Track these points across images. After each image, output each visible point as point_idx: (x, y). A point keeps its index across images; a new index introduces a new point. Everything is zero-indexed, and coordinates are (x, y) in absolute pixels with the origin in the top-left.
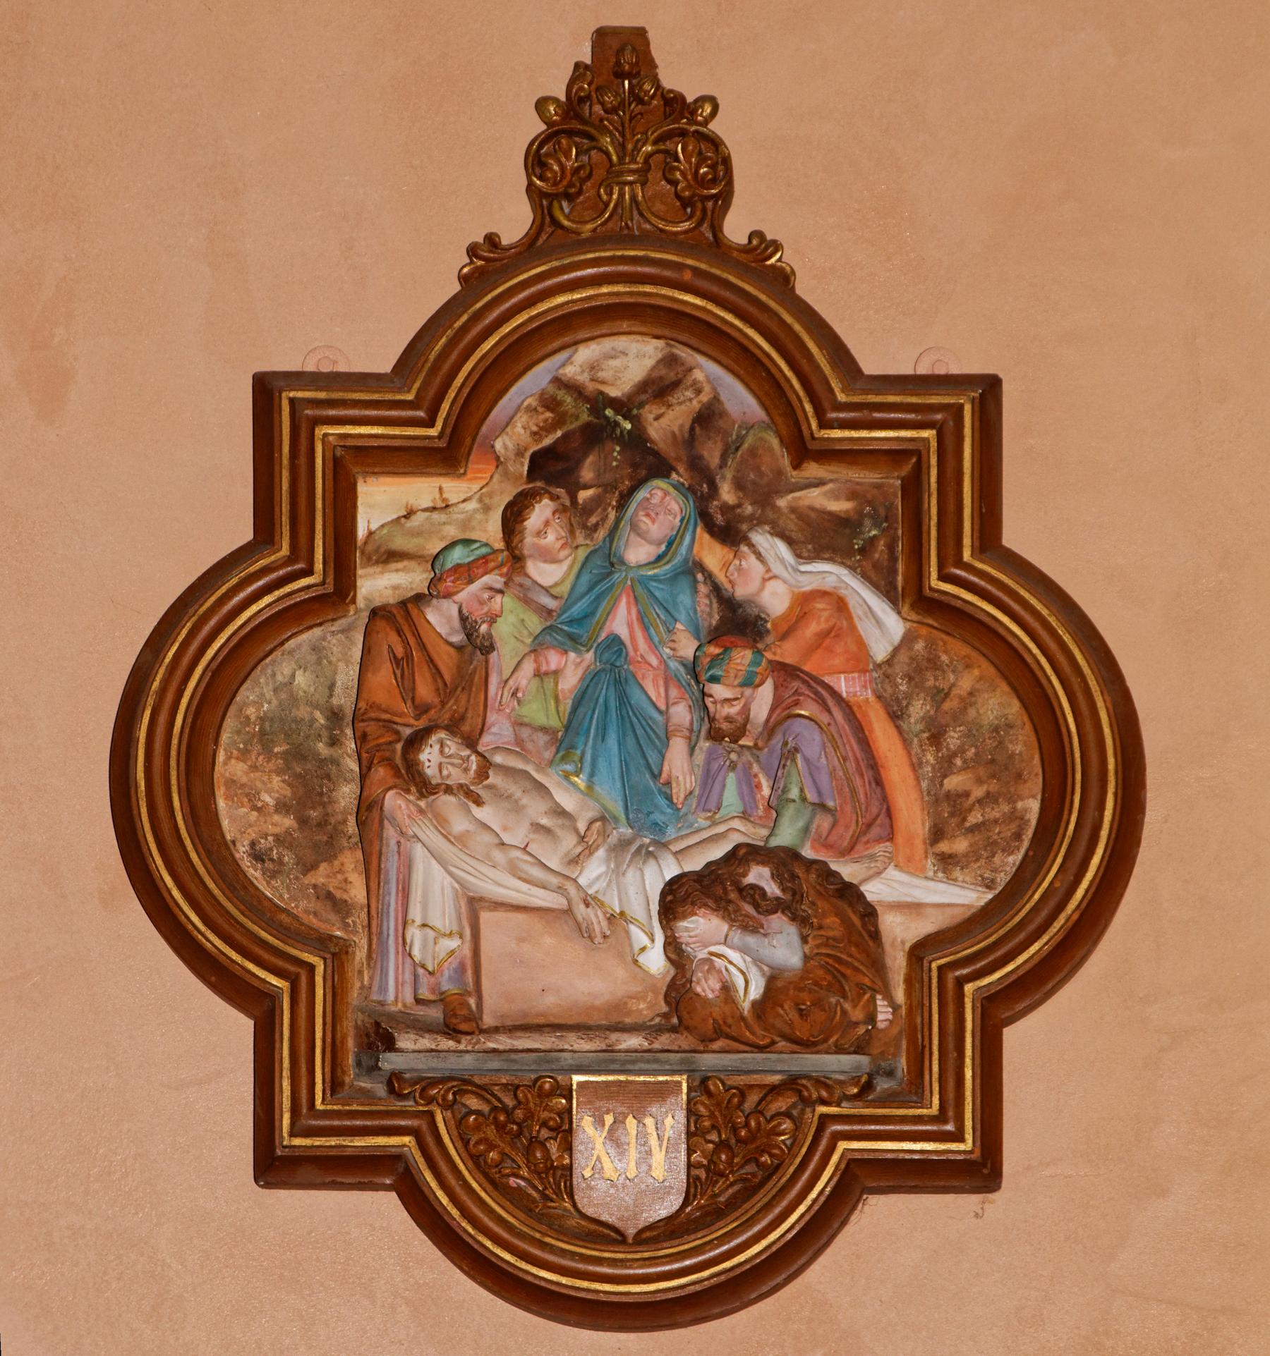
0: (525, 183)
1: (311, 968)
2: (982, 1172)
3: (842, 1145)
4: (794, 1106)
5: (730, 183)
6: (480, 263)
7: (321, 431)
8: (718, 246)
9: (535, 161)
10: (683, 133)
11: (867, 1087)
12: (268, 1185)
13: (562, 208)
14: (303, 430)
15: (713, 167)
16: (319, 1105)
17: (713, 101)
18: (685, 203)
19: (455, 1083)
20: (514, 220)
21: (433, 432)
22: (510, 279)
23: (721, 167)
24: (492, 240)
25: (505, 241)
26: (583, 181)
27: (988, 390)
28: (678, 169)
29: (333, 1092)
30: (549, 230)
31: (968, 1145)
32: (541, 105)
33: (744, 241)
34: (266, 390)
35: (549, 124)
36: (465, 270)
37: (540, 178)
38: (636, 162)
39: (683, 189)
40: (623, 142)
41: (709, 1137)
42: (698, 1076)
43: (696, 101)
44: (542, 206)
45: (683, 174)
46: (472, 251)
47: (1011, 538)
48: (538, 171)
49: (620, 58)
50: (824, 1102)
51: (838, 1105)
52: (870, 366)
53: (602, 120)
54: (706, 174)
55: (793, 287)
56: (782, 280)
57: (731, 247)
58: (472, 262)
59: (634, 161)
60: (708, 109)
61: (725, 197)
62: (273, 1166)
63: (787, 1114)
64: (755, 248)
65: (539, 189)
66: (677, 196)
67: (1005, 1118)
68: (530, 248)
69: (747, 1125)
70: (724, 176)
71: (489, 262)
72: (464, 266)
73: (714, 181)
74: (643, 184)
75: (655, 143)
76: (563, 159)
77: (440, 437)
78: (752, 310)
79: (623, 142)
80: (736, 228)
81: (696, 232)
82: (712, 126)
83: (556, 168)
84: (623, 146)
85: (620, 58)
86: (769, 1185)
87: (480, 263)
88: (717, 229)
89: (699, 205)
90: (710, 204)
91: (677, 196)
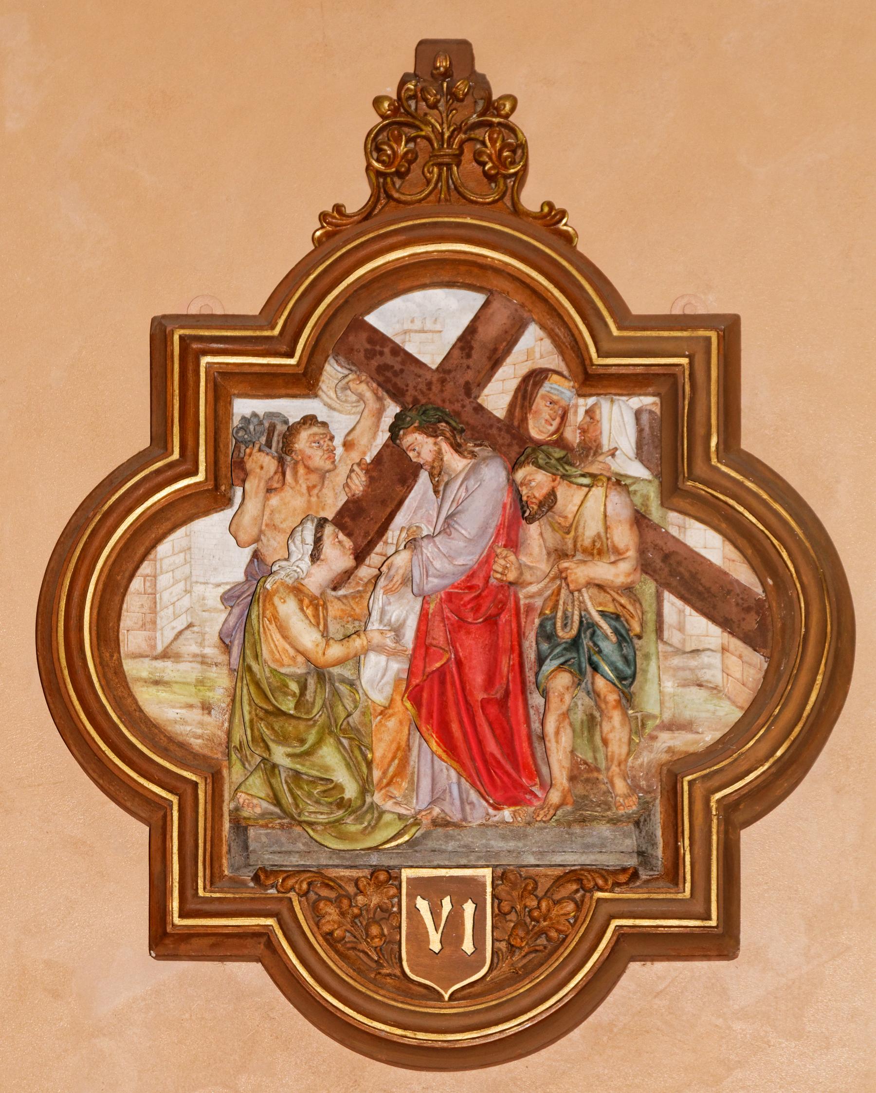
0: (365, 164)
1: (195, 473)
2: (722, 942)
3: (615, 923)
4: (577, 891)
5: (525, 168)
6: (329, 228)
7: (205, 360)
8: (517, 210)
9: (374, 144)
10: (490, 125)
11: (635, 875)
12: (158, 957)
13: (394, 184)
14: (190, 356)
15: (514, 152)
16: (201, 893)
17: (514, 101)
18: (490, 178)
19: (309, 875)
20: (357, 195)
21: (293, 361)
22: (485, 949)
23: (519, 152)
24: (338, 208)
25: (350, 209)
26: (410, 162)
27: (729, 329)
28: (484, 152)
29: (212, 884)
30: (383, 201)
31: (713, 923)
32: (377, 102)
33: (538, 210)
34: (160, 331)
35: (384, 117)
36: (318, 233)
37: (378, 161)
38: (452, 148)
39: (490, 169)
40: (444, 139)
41: (508, 917)
42: (499, 871)
43: (500, 98)
44: (378, 183)
45: (490, 157)
46: (323, 216)
47: (748, 443)
48: (375, 155)
49: (444, 77)
50: (601, 889)
51: (611, 891)
52: (638, 306)
53: (426, 114)
54: (507, 157)
55: (575, 246)
56: (568, 239)
57: (528, 214)
58: (323, 227)
59: (450, 145)
60: (508, 107)
61: (521, 178)
62: (164, 941)
63: (571, 898)
64: (545, 216)
65: (379, 173)
66: (485, 174)
67: (742, 890)
68: (367, 214)
69: (539, 907)
70: (522, 159)
71: (334, 224)
72: (317, 230)
73: (513, 163)
74: (458, 166)
75: (465, 133)
76: (395, 146)
77: (298, 364)
78: (546, 274)
79: (444, 139)
80: (531, 198)
81: (500, 204)
82: (511, 119)
83: (389, 152)
84: (442, 134)
85: (444, 77)
86: (558, 950)
87: (329, 228)
88: (515, 204)
89: (501, 181)
90: (510, 182)
91: (485, 174)
